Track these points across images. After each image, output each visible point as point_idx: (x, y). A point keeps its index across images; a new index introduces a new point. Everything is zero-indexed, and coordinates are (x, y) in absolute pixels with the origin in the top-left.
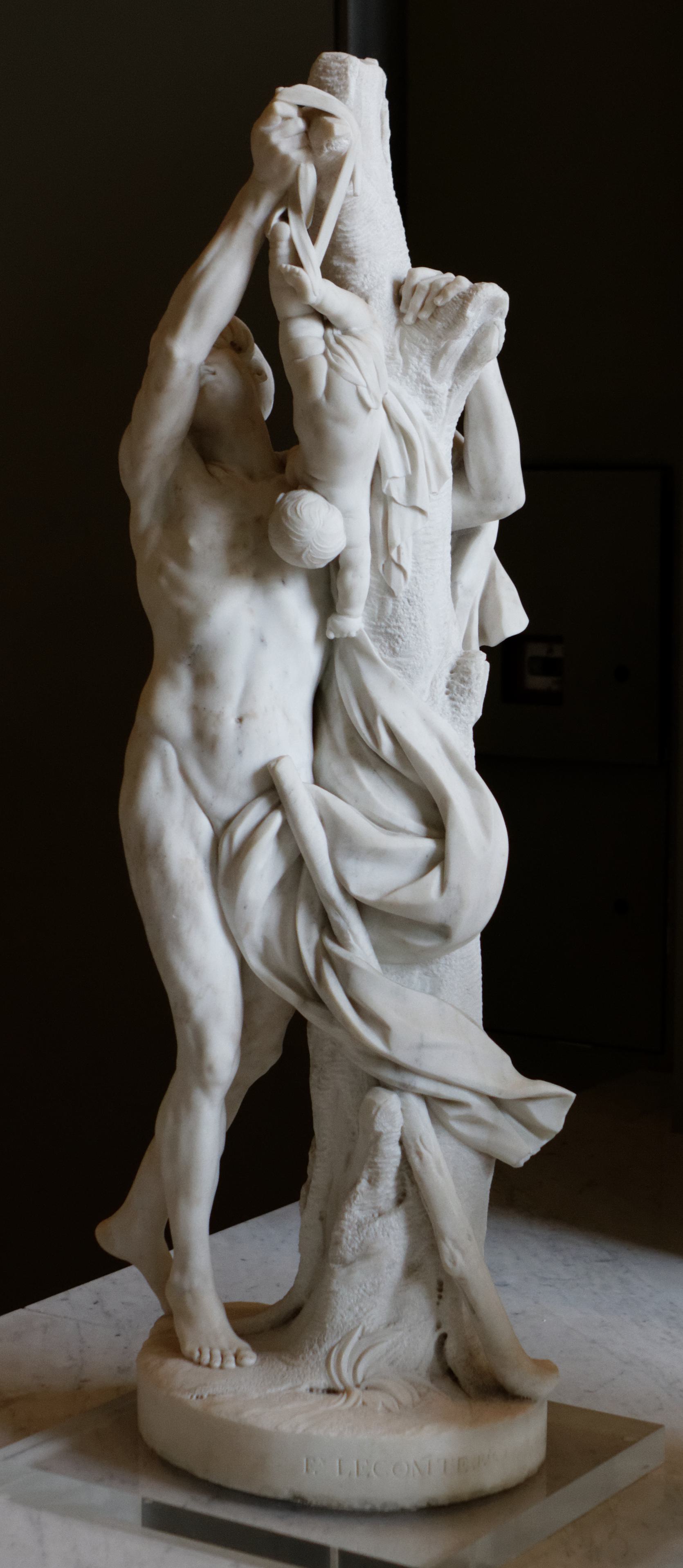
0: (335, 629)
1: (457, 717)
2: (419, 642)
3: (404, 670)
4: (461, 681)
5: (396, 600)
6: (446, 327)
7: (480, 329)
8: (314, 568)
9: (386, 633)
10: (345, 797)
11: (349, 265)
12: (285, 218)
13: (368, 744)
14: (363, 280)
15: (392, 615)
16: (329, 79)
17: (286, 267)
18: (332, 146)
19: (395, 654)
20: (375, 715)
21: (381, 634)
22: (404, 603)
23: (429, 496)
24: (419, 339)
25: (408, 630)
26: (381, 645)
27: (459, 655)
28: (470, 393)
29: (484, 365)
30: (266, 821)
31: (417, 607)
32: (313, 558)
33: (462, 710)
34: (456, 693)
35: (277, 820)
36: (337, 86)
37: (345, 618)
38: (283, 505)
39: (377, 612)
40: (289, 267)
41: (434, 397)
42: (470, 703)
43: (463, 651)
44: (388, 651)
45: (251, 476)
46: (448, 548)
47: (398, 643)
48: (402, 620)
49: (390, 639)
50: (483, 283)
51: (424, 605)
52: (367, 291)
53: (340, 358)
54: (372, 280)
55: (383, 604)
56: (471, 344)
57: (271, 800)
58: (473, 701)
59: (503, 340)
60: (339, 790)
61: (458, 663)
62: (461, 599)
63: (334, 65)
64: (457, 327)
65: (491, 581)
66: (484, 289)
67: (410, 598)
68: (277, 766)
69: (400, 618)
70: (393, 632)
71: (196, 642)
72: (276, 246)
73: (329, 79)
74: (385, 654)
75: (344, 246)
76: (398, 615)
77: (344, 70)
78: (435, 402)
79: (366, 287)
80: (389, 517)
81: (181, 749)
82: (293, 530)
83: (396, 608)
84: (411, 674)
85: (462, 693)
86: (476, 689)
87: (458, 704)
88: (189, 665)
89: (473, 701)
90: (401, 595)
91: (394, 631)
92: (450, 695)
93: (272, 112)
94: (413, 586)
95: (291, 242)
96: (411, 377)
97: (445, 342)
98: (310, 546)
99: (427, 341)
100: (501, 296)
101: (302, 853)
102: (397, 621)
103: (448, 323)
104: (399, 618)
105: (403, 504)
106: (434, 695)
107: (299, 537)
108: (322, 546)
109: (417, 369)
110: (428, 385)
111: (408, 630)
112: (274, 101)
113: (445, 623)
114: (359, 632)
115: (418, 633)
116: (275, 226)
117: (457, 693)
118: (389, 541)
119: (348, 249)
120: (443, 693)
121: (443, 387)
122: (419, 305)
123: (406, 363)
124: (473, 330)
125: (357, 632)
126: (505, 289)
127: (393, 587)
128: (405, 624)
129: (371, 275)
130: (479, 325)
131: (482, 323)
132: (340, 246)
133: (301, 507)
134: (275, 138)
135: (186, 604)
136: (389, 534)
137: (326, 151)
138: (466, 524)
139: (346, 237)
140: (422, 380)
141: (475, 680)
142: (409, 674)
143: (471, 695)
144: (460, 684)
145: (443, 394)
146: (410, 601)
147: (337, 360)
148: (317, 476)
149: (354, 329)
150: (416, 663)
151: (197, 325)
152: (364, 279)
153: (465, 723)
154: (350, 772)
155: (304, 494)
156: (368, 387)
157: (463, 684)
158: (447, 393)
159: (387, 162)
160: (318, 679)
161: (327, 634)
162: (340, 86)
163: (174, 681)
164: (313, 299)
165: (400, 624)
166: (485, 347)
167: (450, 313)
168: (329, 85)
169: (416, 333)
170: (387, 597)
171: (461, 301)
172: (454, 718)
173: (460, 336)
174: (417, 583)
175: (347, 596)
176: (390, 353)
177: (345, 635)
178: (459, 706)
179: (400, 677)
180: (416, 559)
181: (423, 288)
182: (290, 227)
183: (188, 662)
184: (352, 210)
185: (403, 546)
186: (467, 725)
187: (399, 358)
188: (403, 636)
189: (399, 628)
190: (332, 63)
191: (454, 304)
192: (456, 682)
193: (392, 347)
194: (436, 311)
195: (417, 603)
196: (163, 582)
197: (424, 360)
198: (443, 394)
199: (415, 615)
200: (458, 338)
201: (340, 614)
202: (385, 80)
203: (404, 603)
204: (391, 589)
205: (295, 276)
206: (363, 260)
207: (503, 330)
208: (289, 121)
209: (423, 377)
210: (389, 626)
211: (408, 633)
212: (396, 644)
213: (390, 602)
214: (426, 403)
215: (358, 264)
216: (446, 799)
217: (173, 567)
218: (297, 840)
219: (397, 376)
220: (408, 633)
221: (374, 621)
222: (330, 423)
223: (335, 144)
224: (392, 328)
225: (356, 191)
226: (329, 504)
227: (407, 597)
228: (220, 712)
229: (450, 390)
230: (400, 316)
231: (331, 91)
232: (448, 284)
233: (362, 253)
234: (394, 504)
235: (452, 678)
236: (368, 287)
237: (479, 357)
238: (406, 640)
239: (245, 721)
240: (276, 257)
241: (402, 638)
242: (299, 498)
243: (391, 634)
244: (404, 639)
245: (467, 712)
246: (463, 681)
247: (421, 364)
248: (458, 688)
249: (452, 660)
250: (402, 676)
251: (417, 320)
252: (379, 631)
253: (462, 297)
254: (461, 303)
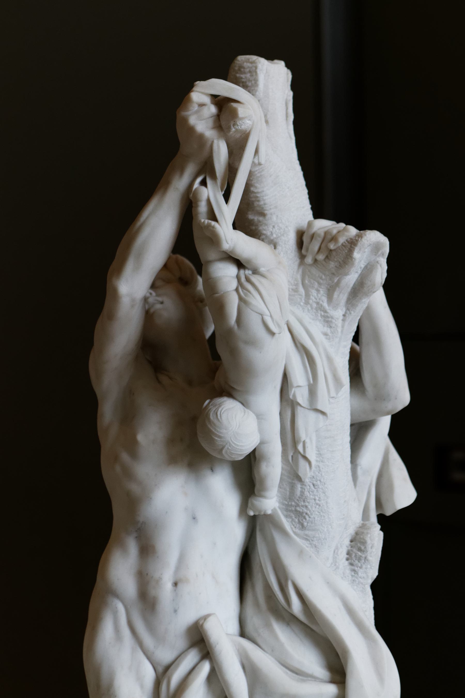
0: (254, 508)
1: (356, 579)
2: (323, 518)
3: (311, 541)
4: (359, 549)
5: (303, 484)
6: (338, 266)
7: (366, 267)
8: (234, 460)
9: (296, 511)
10: (264, 647)
11: (261, 218)
12: (204, 183)
13: (282, 604)
14: (271, 230)
15: (300, 496)
16: (243, 76)
17: (204, 222)
18: (238, 125)
19: (303, 528)
20: (286, 579)
21: (291, 511)
22: (310, 486)
23: (329, 400)
24: (317, 275)
25: (314, 509)
26: (292, 520)
27: (358, 526)
28: (361, 316)
29: (370, 295)
30: (196, 668)
31: (321, 490)
32: (232, 454)
33: (360, 574)
34: (354, 559)
35: (206, 667)
36: (250, 81)
37: (261, 499)
38: (208, 410)
39: (288, 493)
40: (206, 221)
41: (331, 322)
42: (366, 568)
43: (362, 522)
44: (298, 525)
45: (190, 383)
46: (347, 439)
47: (305, 519)
48: (308, 501)
49: (299, 516)
50: (367, 230)
51: (327, 488)
52: (275, 238)
53: (249, 293)
54: (279, 230)
55: (292, 487)
56: (359, 279)
57: (201, 650)
58: (369, 566)
59: (385, 275)
60: (259, 640)
61: (357, 533)
62: (361, 478)
63: (246, 65)
64: (347, 266)
65: (385, 462)
66: (367, 236)
67: (315, 482)
68: (205, 623)
69: (307, 499)
70: (301, 510)
71: (141, 519)
72: (197, 206)
73: (243, 76)
74: (295, 527)
75: (256, 204)
76: (305, 497)
77: (254, 68)
78: (331, 325)
79: (275, 236)
80: (296, 417)
81: (129, 607)
83: (303, 490)
84: (317, 544)
85: (359, 559)
86: (371, 556)
87: (356, 568)
88: (136, 537)
89: (369, 566)
90: (307, 481)
91: (302, 509)
92: (350, 561)
93: (190, 100)
94: (317, 473)
95: (209, 202)
96: (311, 306)
97: (337, 278)
98: (228, 444)
99: (324, 277)
100: (382, 241)
101: (227, 695)
102: (304, 501)
103: (340, 263)
104: (306, 499)
105: (307, 407)
106: (336, 562)
107: (219, 437)
108: (238, 444)
109: (316, 299)
110: (325, 311)
111: (314, 509)
112: (192, 92)
113: (345, 502)
114: (274, 510)
115: (322, 511)
116: (196, 189)
117: (356, 559)
118: (296, 437)
119: (259, 206)
120: (344, 560)
121: (338, 313)
122: (316, 248)
123: (307, 295)
124: (361, 268)
125: (272, 510)
126: (385, 235)
127: (300, 474)
128: (311, 504)
129: (278, 226)
130: (365, 264)
131: (367, 262)
132: (253, 204)
133: (221, 412)
134: (192, 120)
135: (134, 488)
136: (296, 432)
137: (233, 130)
138: (364, 418)
139: (257, 197)
140: (320, 307)
141: (370, 549)
142: (315, 544)
143: (366, 561)
144: (357, 552)
145: (338, 319)
146: (315, 485)
147: (246, 295)
148: (235, 387)
149: (262, 270)
150: (320, 535)
151: (137, 268)
152: (273, 229)
153: (362, 584)
154: (268, 626)
155: (225, 401)
156: (271, 316)
157: (360, 552)
158: (341, 317)
159: (291, 138)
160: (244, 546)
161: (248, 512)
162: (251, 81)
164: (226, 246)
165: (307, 504)
166: (370, 281)
167: (341, 255)
168: (243, 80)
169: (314, 271)
170: (296, 482)
171: (349, 245)
172: (353, 580)
173: (350, 273)
174: (320, 470)
175: (262, 481)
176: (294, 287)
177: (262, 513)
178: (357, 571)
179: (307, 547)
180: (318, 451)
181: (319, 236)
182: (208, 189)
183: (135, 535)
184: (261, 175)
185: (308, 441)
186: (364, 586)
187: (302, 290)
188: (309, 514)
189: (306, 507)
190: (245, 64)
191: (343, 247)
192: (355, 550)
193: (296, 282)
194: (330, 254)
195: (320, 487)
197: (322, 292)
198: (338, 319)
199: (319, 496)
200: (349, 274)
201: (258, 496)
202: (290, 76)
203: (310, 486)
204: (299, 476)
205: (212, 229)
206: (271, 214)
207: (385, 267)
208: (204, 107)
209: (321, 305)
210: (298, 505)
211: (313, 511)
212: (304, 520)
213: (299, 486)
214: (324, 326)
215: (267, 217)
216: (346, 651)
217: (125, 457)
218: (223, 684)
219: (301, 305)
220: (313, 511)
221: (286, 501)
222: (241, 345)
223: (240, 124)
224: (296, 267)
225: (260, 161)
226: (245, 409)
227: (312, 482)
228: (159, 577)
229: (344, 315)
230: (302, 257)
231: (245, 86)
232: (339, 232)
233: (270, 209)
234: (299, 408)
235: (352, 547)
236: (276, 235)
237: (365, 289)
238: (312, 517)
239: (179, 585)
240: (197, 214)
241: (308, 515)
242: (220, 405)
243: (300, 512)
244: (310, 516)
245: (364, 575)
246: (360, 550)
247: (320, 295)
248: (356, 556)
249: (351, 531)
250: (310, 546)
251: (315, 261)
252: (291, 509)
253: (350, 242)
254: (349, 247)
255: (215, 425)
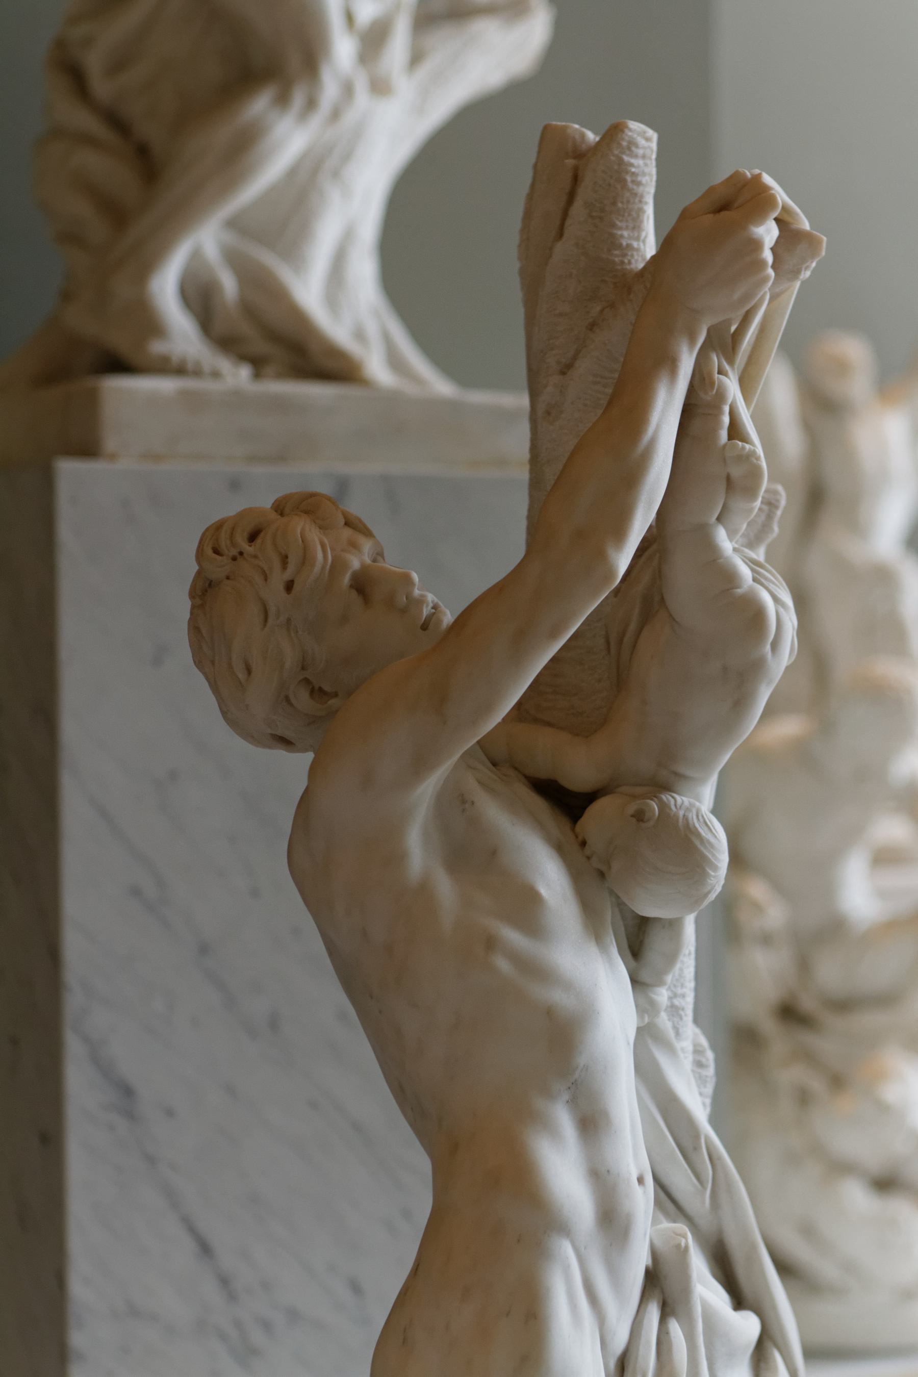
20: (697, 1148)
36: (644, 174)
82: (710, 856)
124: (255, 546)
135: (558, 997)
148: (688, 772)
163: (554, 1133)
196: (502, 964)
217: (512, 936)
255: (712, 846)
